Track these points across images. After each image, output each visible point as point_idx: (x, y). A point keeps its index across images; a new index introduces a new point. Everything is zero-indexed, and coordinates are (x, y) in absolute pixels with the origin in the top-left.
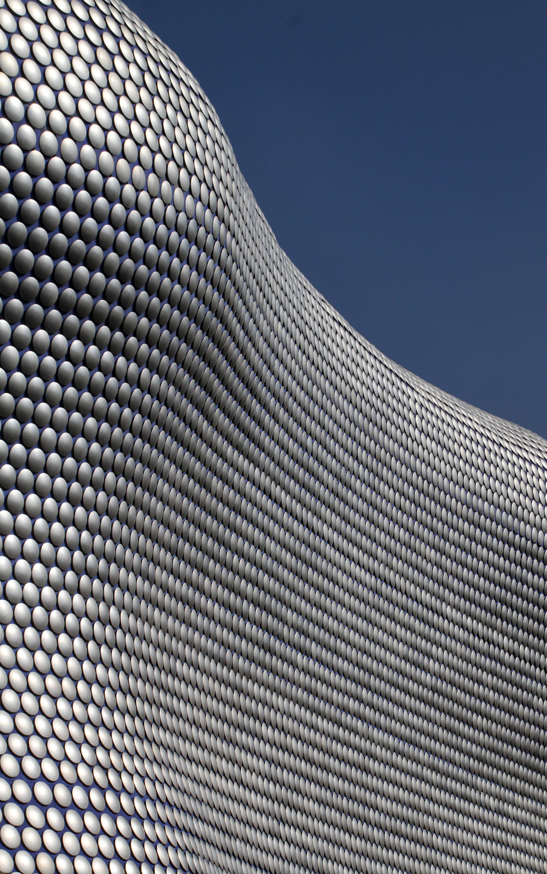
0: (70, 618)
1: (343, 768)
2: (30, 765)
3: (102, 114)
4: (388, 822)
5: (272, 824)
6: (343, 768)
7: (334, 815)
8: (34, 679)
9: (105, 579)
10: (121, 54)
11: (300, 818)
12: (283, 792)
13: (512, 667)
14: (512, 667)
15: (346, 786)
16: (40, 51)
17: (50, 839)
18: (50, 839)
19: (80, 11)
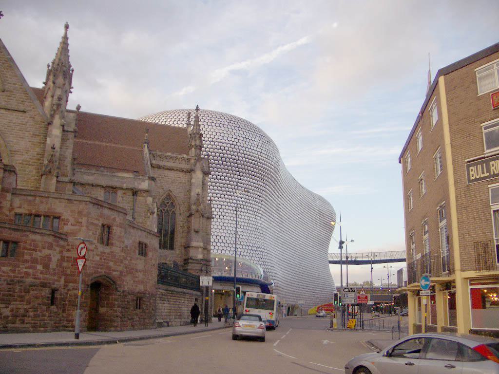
18: (251, 255)
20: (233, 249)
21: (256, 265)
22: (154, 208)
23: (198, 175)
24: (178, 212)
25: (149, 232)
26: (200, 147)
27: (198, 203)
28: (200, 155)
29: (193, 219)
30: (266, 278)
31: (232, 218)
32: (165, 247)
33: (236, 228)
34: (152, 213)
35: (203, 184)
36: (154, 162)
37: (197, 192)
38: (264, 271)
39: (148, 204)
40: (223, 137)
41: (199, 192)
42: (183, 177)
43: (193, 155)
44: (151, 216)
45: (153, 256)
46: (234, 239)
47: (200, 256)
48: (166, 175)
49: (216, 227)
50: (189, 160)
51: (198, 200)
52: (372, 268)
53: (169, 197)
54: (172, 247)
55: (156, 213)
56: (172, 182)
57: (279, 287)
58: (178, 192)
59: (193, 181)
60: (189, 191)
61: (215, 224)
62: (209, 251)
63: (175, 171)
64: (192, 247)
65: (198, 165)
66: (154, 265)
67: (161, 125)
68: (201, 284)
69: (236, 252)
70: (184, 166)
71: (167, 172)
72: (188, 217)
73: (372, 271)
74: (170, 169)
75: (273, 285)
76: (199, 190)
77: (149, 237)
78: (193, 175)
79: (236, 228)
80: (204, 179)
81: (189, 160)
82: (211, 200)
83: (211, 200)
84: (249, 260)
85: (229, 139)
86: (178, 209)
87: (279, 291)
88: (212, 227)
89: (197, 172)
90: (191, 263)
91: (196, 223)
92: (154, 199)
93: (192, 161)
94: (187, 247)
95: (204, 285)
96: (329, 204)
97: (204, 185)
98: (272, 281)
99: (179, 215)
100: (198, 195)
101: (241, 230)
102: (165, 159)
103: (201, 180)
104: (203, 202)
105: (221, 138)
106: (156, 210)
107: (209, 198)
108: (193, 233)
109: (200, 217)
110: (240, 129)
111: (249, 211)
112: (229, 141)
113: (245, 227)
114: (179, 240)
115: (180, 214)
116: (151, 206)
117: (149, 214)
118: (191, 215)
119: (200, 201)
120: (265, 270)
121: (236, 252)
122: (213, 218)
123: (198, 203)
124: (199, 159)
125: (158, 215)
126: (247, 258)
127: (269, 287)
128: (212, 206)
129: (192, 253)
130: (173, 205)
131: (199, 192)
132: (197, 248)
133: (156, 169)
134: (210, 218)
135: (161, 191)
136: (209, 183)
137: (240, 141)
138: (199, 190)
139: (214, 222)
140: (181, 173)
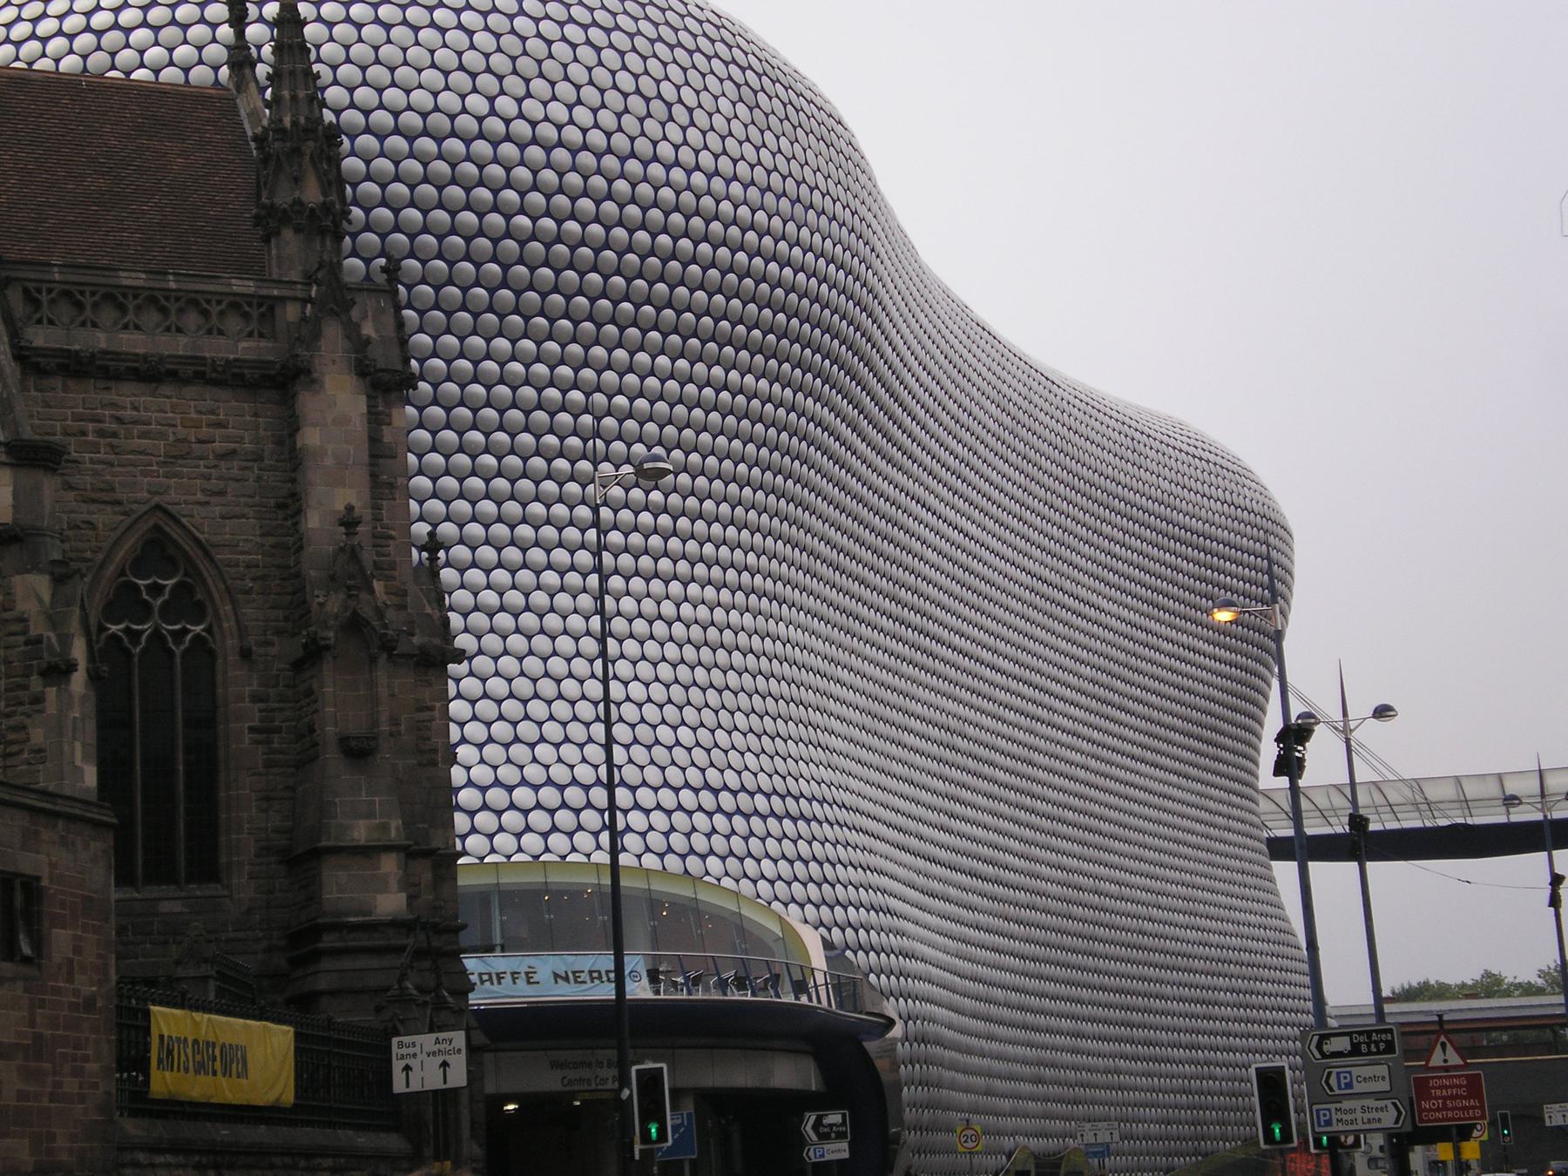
0: (742, 637)
1: (1008, 762)
2: (712, 775)
3: (748, 149)
4: (1055, 811)
5: (944, 819)
6: (1008, 762)
7: (1003, 808)
8: (712, 696)
9: (773, 598)
10: (763, 90)
11: (970, 812)
12: (952, 789)
13: (1170, 655)
14: (1170, 655)
15: (1016, 670)
16: (688, 95)
17: (736, 843)
18: (736, 843)
19: (578, 13)
20: (591, 819)
21: (776, 905)
22: (66, 641)
23: (335, 406)
24: (232, 643)
25: (48, 810)
26: (328, 223)
27: (351, 571)
28: (335, 268)
29: (331, 685)
30: (847, 986)
31: (573, 579)
32: (161, 873)
33: (605, 682)
34: (59, 671)
35: (373, 456)
36: (39, 337)
37: (340, 507)
38: (828, 945)
39: (22, 620)
40: (491, 100)
41: (350, 508)
42: (239, 420)
43: (295, 275)
44: (51, 692)
45: (77, 950)
46: (595, 753)
47: (391, 903)
48: (128, 413)
49: (481, 774)
50: (268, 307)
51: (353, 554)
52: (1556, 880)
53: (161, 546)
54: (206, 867)
55: (82, 665)
56: (165, 454)
57: (939, 1042)
58: (225, 525)
59: (310, 437)
60: (291, 505)
61: (468, 702)
62: (445, 861)
63: (185, 382)
64: (337, 850)
65: (332, 332)
66: (89, 1004)
67: (55, 81)
68: (399, 1086)
69: (615, 835)
70: (245, 348)
71: (130, 398)
72: (297, 666)
73: (1555, 901)
74: (151, 373)
75: (897, 1031)
76: (350, 495)
77: (46, 835)
78: (308, 403)
79: (605, 682)
80: (376, 419)
81: (268, 307)
82: (433, 544)
83: (433, 544)
84: (727, 882)
85: (532, 108)
86: (229, 624)
87: (933, 1070)
88: (458, 708)
89: (328, 381)
90: (336, 953)
91: (338, 703)
92: (59, 581)
93: (291, 312)
94: (302, 857)
95: (415, 1086)
96: (1238, 474)
97: (383, 468)
98: (890, 1008)
99: (233, 658)
100: (349, 522)
101: (637, 690)
102: (108, 315)
103: (359, 425)
104: (385, 569)
105: (477, 103)
106: (79, 651)
107: (421, 529)
108: (332, 757)
109: (373, 660)
110: (596, 35)
111: (700, 569)
112: (534, 124)
113: (665, 671)
114: (247, 819)
115: (246, 654)
116: (37, 628)
117: (36, 682)
118: (314, 653)
119: (368, 557)
120: (836, 934)
121: (615, 835)
122: (460, 656)
123: (351, 571)
124: (337, 297)
125: (94, 677)
126: (713, 863)
127: (871, 1046)
128: (448, 575)
129: (340, 887)
130: (188, 602)
131: (350, 508)
132: (368, 852)
133: (57, 382)
134: (437, 656)
135: (104, 517)
136: (422, 482)
137: (606, 118)
138: (350, 495)
139: (463, 680)
140: (224, 394)
